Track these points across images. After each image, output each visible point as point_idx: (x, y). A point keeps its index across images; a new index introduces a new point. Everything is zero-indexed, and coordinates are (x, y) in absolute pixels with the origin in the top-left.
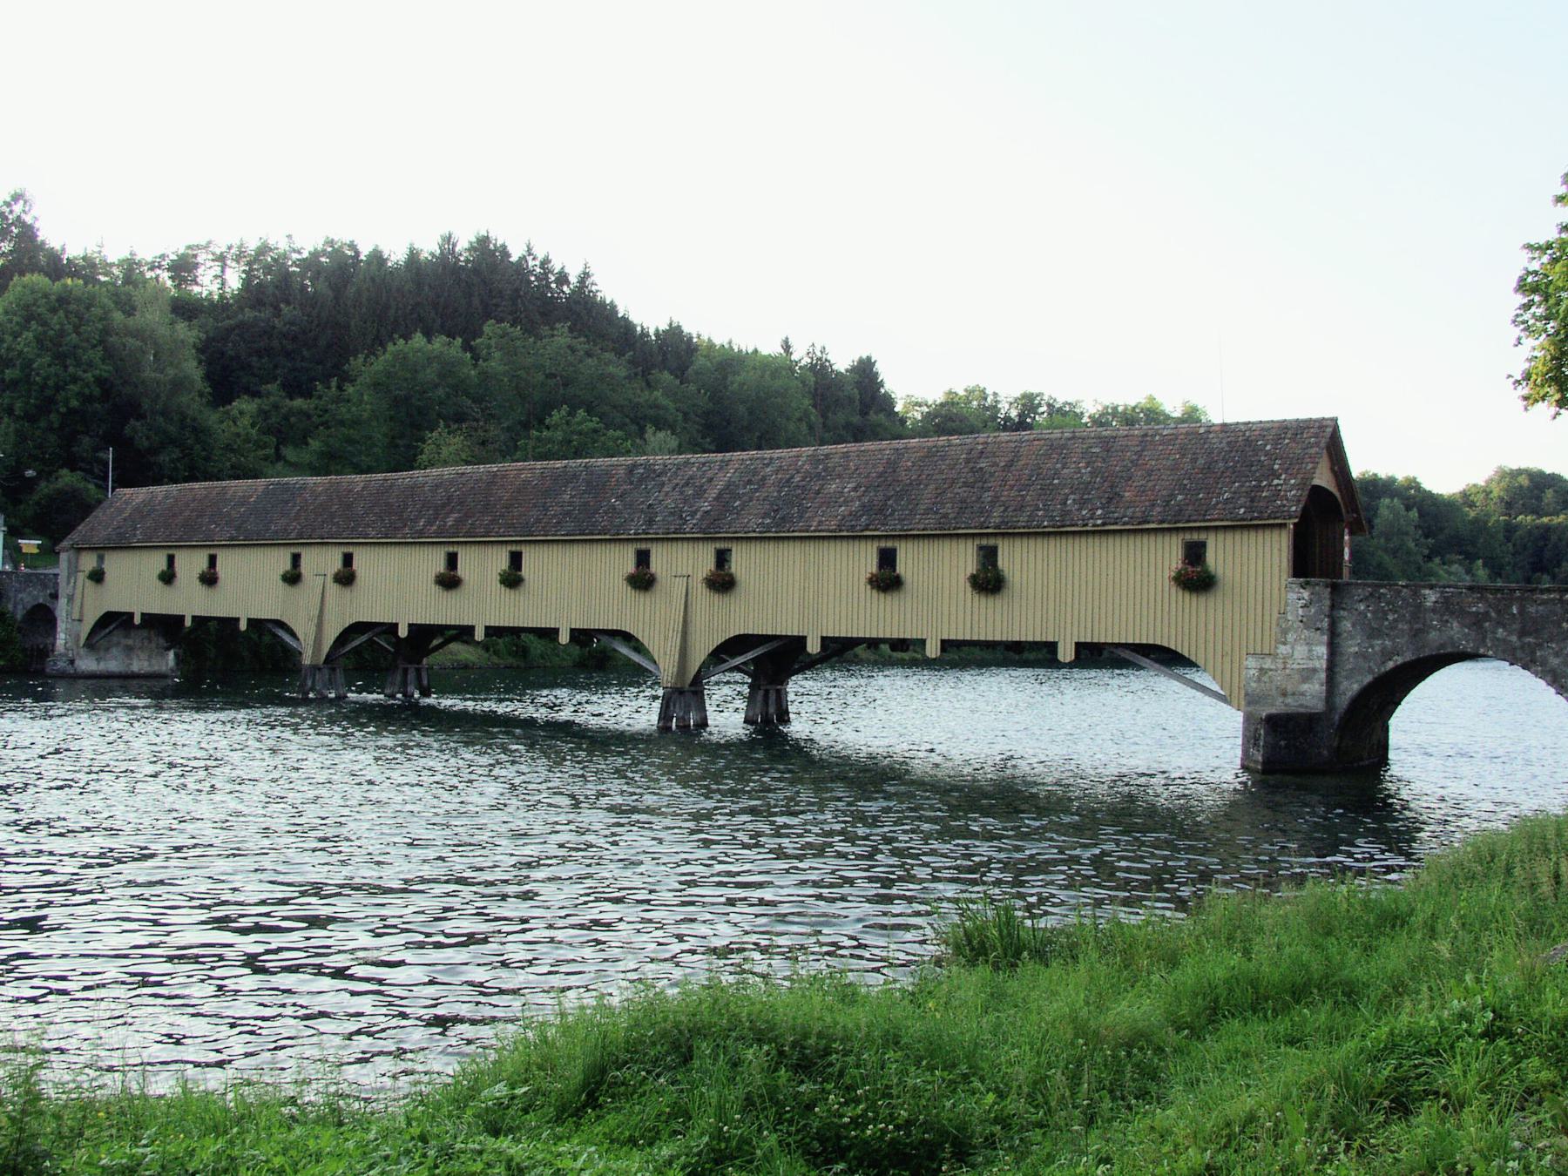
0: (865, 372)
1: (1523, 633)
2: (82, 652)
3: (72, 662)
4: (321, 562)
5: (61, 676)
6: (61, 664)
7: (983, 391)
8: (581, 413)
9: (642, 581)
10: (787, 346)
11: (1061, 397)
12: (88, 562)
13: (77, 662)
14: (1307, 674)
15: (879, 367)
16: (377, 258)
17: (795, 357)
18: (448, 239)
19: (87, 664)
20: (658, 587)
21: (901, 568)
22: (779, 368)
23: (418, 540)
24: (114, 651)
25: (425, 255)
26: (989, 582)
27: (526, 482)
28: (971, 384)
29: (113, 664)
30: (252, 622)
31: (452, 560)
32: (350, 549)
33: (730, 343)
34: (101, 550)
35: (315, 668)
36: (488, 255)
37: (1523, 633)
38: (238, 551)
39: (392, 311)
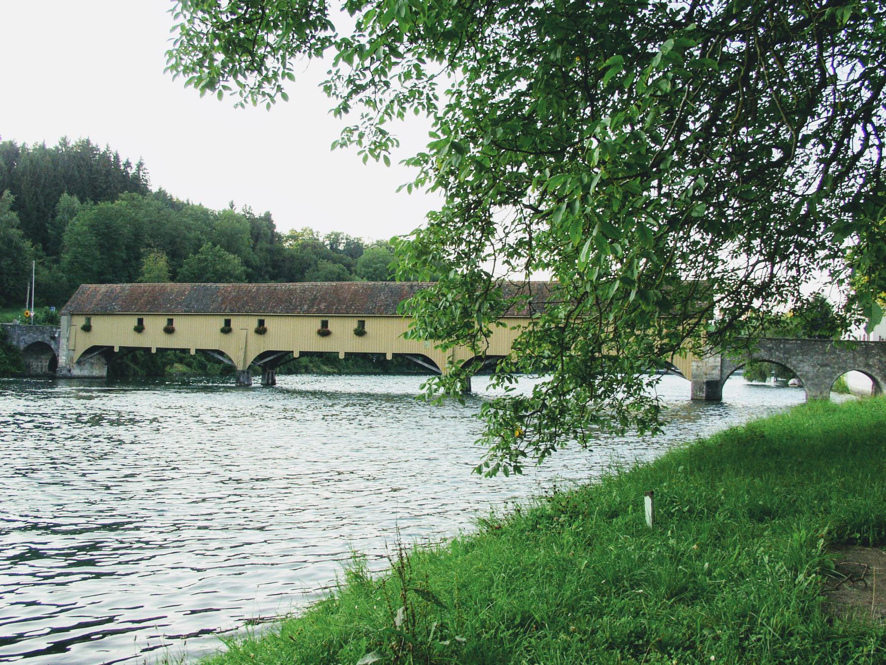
0: (268, 217)
1: (784, 353)
2: (75, 366)
3: (70, 371)
4: (244, 325)
5: (65, 377)
6: (64, 372)
7: (311, 230)
8: (218, 246)
9: (227, 329)
10: (232, 206)
11: (353, 235)
12: (81, 321)
13: (72, 371)
14: (714, 368)
15: (273, 218)
16: (24, 148)
17: (236, 212)
18: (64, 139)
19: (76, 372)
20: (175, 334)
21: (330, 328)
22: (229, 216)
23: (307, 314)
24: (87, 365)
25: (47, 147)
26: (169, 330)
27: (356, 291)
28: (305, 226)
29: (86, 373)
30: (159, 350)
31: (170, 321)
32: (263, 318)
33: (188, 201)
34: (88, 316)
35: (243, 372)
36: (86, 147)
37: (784, 353)
38: (190, 317)
39: (42, 181)
